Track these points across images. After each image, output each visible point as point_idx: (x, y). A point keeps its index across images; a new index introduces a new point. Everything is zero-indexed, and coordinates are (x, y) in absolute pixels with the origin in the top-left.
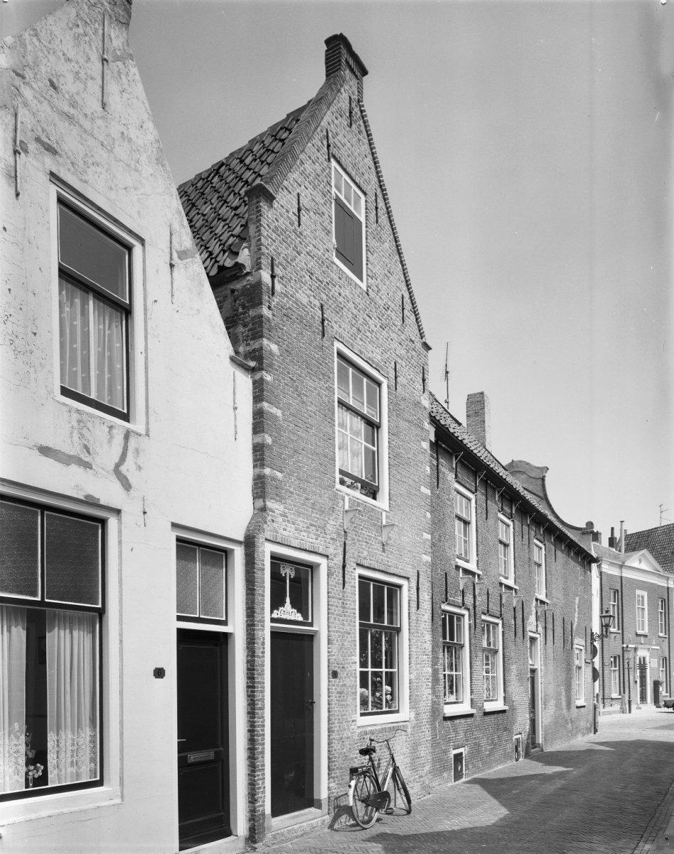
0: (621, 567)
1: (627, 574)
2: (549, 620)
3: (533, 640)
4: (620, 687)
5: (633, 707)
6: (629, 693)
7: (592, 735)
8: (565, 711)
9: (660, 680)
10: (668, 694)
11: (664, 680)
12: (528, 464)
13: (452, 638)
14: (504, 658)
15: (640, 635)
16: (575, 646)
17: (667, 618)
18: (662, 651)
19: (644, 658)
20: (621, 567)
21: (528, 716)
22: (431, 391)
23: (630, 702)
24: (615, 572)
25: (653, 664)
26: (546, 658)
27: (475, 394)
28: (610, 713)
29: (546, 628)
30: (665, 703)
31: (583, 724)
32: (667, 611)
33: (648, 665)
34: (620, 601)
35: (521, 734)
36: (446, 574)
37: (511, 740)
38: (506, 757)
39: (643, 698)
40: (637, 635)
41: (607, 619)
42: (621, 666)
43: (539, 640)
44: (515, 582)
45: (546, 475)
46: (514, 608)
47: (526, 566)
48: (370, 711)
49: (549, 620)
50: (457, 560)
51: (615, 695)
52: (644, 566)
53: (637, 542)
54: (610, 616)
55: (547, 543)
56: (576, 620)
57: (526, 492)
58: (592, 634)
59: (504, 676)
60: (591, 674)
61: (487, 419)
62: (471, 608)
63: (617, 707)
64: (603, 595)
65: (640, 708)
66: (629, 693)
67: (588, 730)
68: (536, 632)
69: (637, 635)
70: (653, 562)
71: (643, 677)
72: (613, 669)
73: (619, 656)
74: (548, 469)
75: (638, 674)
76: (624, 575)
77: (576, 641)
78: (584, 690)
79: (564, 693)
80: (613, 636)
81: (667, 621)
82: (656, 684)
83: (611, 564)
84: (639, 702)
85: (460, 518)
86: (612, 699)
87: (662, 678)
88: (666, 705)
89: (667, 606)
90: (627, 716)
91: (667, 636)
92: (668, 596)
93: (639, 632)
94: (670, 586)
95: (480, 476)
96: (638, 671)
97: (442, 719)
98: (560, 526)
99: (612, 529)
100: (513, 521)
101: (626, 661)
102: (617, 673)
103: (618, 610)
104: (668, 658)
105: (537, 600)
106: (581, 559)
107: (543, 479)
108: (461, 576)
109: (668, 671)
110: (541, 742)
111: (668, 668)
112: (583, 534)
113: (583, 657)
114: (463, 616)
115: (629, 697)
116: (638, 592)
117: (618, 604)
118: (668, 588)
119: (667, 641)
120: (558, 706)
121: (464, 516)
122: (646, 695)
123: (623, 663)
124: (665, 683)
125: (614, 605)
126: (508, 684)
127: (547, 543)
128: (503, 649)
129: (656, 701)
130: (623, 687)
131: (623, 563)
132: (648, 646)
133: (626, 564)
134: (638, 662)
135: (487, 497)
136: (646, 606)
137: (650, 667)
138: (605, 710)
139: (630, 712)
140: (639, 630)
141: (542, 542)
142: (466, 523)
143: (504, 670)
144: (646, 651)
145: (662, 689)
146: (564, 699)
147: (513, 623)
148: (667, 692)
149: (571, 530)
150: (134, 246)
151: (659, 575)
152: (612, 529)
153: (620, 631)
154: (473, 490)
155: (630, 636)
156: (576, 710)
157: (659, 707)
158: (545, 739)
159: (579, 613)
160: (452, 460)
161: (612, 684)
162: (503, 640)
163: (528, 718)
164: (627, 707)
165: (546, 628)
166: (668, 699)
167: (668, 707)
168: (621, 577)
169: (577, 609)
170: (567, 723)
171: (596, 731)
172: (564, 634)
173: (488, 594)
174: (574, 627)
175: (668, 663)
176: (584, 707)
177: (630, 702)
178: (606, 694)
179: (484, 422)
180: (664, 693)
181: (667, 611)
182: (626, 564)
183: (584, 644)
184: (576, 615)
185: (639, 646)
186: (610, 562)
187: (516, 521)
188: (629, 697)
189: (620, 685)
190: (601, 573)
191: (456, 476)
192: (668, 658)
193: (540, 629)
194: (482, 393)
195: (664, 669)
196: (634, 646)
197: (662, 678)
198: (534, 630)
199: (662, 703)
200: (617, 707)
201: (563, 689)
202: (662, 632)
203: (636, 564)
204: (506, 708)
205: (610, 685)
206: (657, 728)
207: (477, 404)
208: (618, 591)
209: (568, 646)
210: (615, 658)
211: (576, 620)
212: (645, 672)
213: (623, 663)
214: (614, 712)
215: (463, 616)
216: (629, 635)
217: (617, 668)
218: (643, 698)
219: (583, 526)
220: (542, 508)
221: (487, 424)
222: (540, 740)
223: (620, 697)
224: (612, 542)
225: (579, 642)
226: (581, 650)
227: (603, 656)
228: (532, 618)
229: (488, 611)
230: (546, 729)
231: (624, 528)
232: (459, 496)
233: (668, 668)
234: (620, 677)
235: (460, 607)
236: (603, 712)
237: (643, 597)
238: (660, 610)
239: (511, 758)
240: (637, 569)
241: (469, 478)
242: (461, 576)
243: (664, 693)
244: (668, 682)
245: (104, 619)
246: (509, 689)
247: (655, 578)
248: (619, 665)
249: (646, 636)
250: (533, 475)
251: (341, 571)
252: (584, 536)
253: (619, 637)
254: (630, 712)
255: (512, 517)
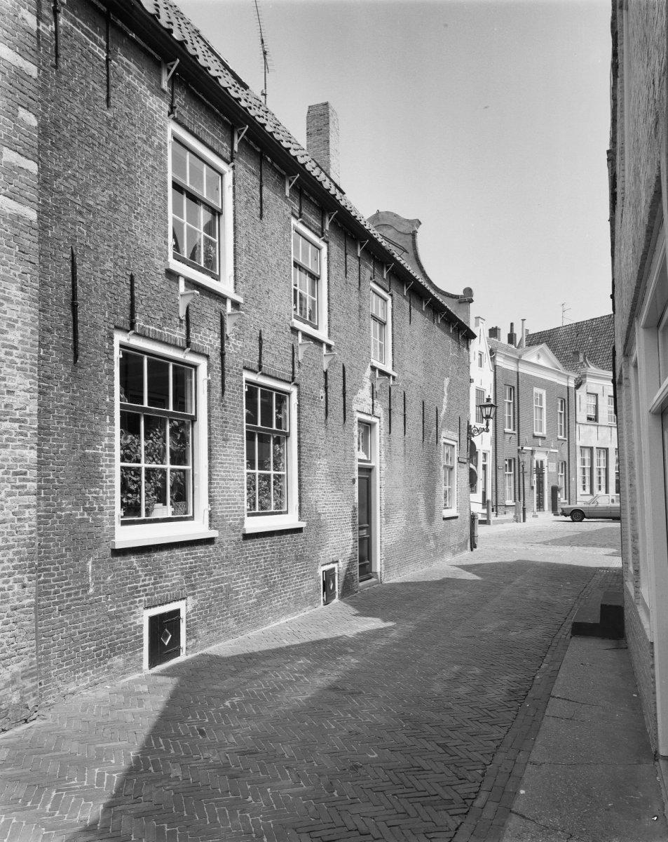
0: (518, 361)
1: (523, 369)
2: (398, 401)
3: (367, 427)
4: (515, 493)
5: (528, 515)
6: (524, 499)
7: (467, 553)
8: (424, 525)
9: (559, 486)
10: (567, 501)
11: (564, 486)
12: (396, 216)
13: (267, 420)
14: (299, 447)
15: (538, 437)
16: (442, 441)
17: (567, 420)
18: (562, 454)
19: (542, 462)
20: (518, 361)
21: (350, 534)
22: (198, 28)
23: (524, 509)
24: (511, 366)
25: (550, 469)
26: (389, 451)
27: (317, 106)
28: (502, 522)
29: (390, 410)
30: (563, 511)
31: (454, 540)
32: (567, 412)
33: (546, 469)
34: (516, 398)
35: (337, 562)
36: (132, 277)
37: (314, 572)
38: (302, 601)
39: (540, 505)
40: (534, 436)
41: (488, 409)
42: (517, 471)
43: (378, 425)
44: (329, 335)
45: (418, 230)
46: (326, 373)
47: (354, 318)
48: (257, 511)
49: (398, 401)
50: (294, 320)
51: (509, 502)
52: (542, 362)
53: (534, 340)
54: (492, 406)
55: (395, 295)
56: (445, 407)
57: (383, 240)
58: (469, 427)
59: (299, 475)
60: (468, 477)
61: (332, 139)
62: (214, 355)
63: (511, 515)
64: (497, 392)
65: (537, 516)
66: (524, 499)
67: (462, 547)
68: (372, 414)
69: (534, 437)
70: (554, 361)
71: (540, 483)
72: (508, 473)
73: (514, 459)
74: (420, 223)
75: (535, 479)
76: (520, 370)
77: (443, 434)
78: (459, 500)
79: (422, 501)
80: (507, 437)
81: (567, 423)
82: (555, 490)
83: (507, 357)
84: (535, 509)
85: (375, 318)
86: (506, 506)
87: (561, 483)
88: (564, 514)
89: (567, 407)
90: (520, 525)
91: (566, 439)
92: (568, 397)
93: (537, 433)
94: (570, 385)
95: (239, 136)
96: (535, 475)
97: (109, 553)
98: (432, 292)
99: (512, 324)
100: (391, 295)
101: (522, 464)
102: (512, 477)
103: (514, 407)
104: (567, 462)
105: (373, 368)
106: (454, 330)
107: (414, 235)
108: (377, 376)
109: (567, 476)
110: (378, 570)
111: (567, 473)
112: (460, 302)
113: (456, 456)
114: (289, 394)
115: (524, 505)
116: (536, 390)
117: (514, 401)
118: (568, 388)
119: (567, 443)
120: (411, 518)
121: (380, 316)
122: (543, 502)
123: (519, 467)
124: (564, 489)
125: (509, 403)
126: (306, 487)
127: (395, 295)
128: (299, 433)
129: (554, 508)
130: (519, 493)
131: (520, 357)
132: (547, 449)
133: (522, 358)
134: (535, 466)
135: (261, 181)
136: (544, 406)
137: (548, 472)
138: (497, 518)
139: (524, 521)
140: (537, 431)
141: (387, 292)
142: (315, 278)
143: (299, 466)
144: (544, 455)
145: (561, 497)
146: (422, 509)
147: (324, 395)
148: (566, 499)
149: (446, 298)
150: (322, 248)
151: (559, 373)
152: (512, 324)
153: (516, 432)
154: (227, 155)
155: (527, 437)
156: (443, 522)
157: (556, 515)
158: (387, 566)
159: (449, 399)
160: (284, 187)
161: (507, 489)
162: (299, 419)
163: (351, 537)
164: (522, 514)
165: (390, 410)
166: (567, 506)
167: (566, 516)
168: (518, 373)
169: (446, 394)
170: (428, 541)
171: (473, 546)
172: (423, 422)
173: (260, 339)
174: (442, 415)
175: (567, 468)
176: (456, 517)
177: (524, 509)
178: (499, 501)
179: (328, 142)
180: (562, 500)
181: (567, 412)
182: (522, 358)
183: (457, 439)
184: (445, 400)
185: (536, 449)
186: (506, 356)
187: (331, 243)
188: (524, 505)
189: (515, 491)
190: (495, 367)
191: (172, 108)
192: (567, 462)
193: (379, 410)
194: (326, 104)
195: (564, 474)
196: (530, 449)
197: (561, 483)
198: (368, 409)
199: (559, 511)
200: (511, 515)
201: (421, 496)
202: (561, 435)
203: (534, 360)
204: (303, 525)
205: (504, 491)
206: (545, 543)
207: (319, 118)
208: (514, 387)
209: (432, 439)
210: (510, 461)
211: (445, 407)
212: (543, 477)
213: (519, 467)
214: (507, 521)
215: (289, 394)
216: (525, 437)
217: (512, 473)
218: (540, 505)
219: (461, 293)
220: (410, 268)
221: (332, 145)
222: (378, 565)
223: (514, 504)
224: (511, 338)
225: (448, 436)
226: (453, 446)
227: (496, 458)
228: (365, 393)
229: (260, 367)
230: (388, 552)
231: (525, 328)
232: (374, 296)
233: (567, 473)
234: (515, 482)
235: (183, 349)
236: (494, 521)
237: (541, 395)
238: (559, 411)
239: (313, 602)
240: (535, 364)
241: (213, 131)
242: (377, 376)
243: (562, 500)
244: (567, 488)
245: (195, 426)
246: (311, 496)
247: (555, 376)
248: (515, 470)
249: (544, 438)
250: (401, 230)
251: (342, 398)
252: (461, 305)
253: (515, 438)
254: (524, 521)
255: (323, 234)
